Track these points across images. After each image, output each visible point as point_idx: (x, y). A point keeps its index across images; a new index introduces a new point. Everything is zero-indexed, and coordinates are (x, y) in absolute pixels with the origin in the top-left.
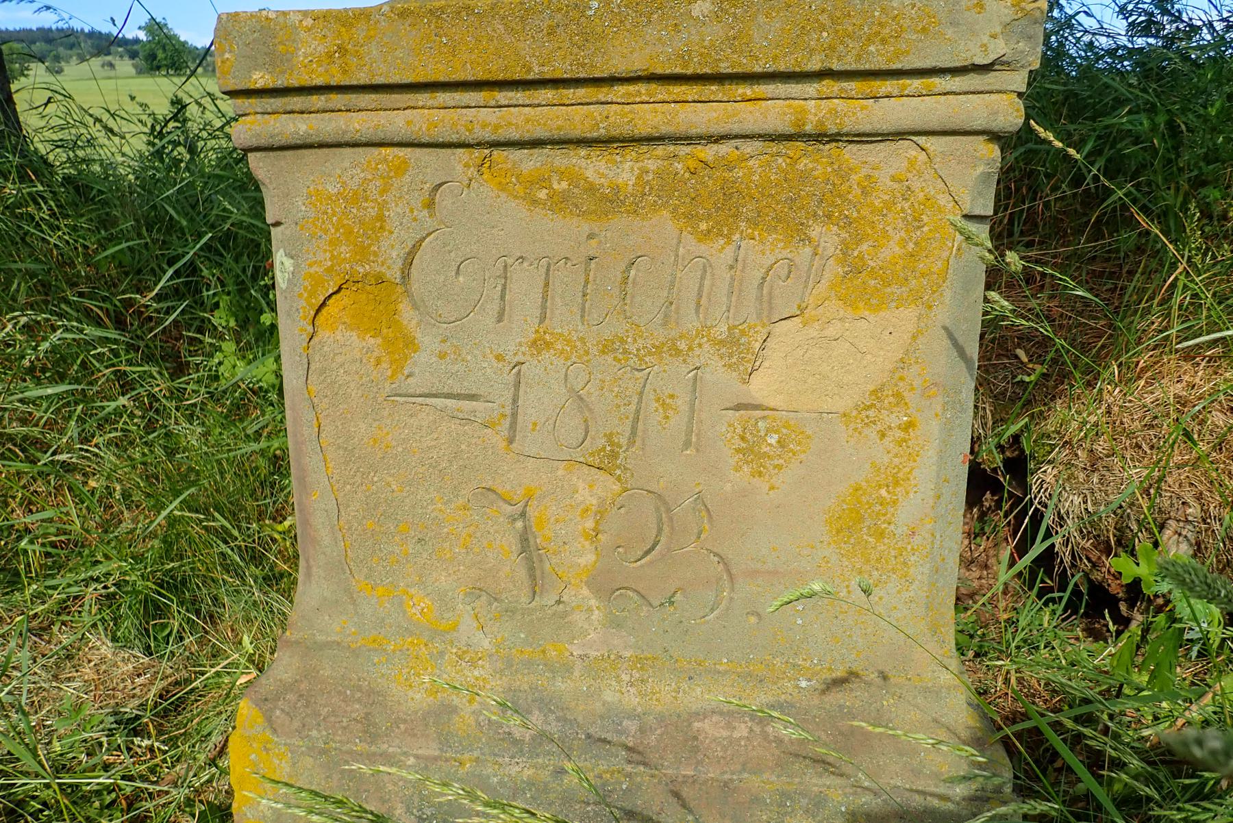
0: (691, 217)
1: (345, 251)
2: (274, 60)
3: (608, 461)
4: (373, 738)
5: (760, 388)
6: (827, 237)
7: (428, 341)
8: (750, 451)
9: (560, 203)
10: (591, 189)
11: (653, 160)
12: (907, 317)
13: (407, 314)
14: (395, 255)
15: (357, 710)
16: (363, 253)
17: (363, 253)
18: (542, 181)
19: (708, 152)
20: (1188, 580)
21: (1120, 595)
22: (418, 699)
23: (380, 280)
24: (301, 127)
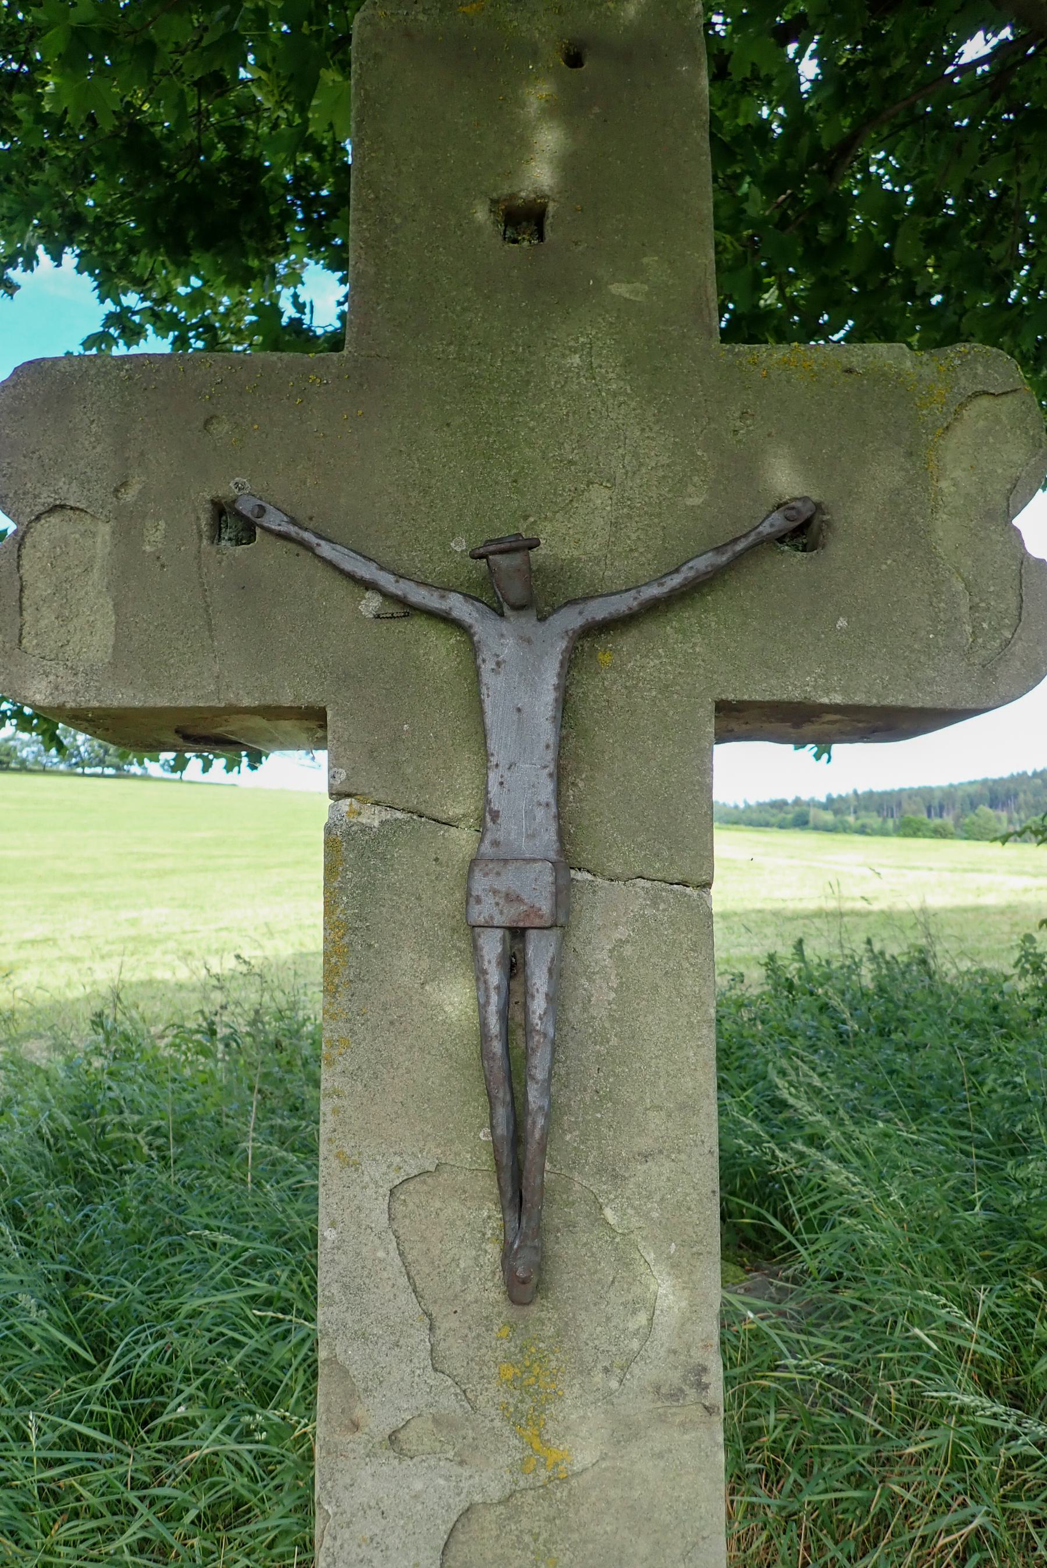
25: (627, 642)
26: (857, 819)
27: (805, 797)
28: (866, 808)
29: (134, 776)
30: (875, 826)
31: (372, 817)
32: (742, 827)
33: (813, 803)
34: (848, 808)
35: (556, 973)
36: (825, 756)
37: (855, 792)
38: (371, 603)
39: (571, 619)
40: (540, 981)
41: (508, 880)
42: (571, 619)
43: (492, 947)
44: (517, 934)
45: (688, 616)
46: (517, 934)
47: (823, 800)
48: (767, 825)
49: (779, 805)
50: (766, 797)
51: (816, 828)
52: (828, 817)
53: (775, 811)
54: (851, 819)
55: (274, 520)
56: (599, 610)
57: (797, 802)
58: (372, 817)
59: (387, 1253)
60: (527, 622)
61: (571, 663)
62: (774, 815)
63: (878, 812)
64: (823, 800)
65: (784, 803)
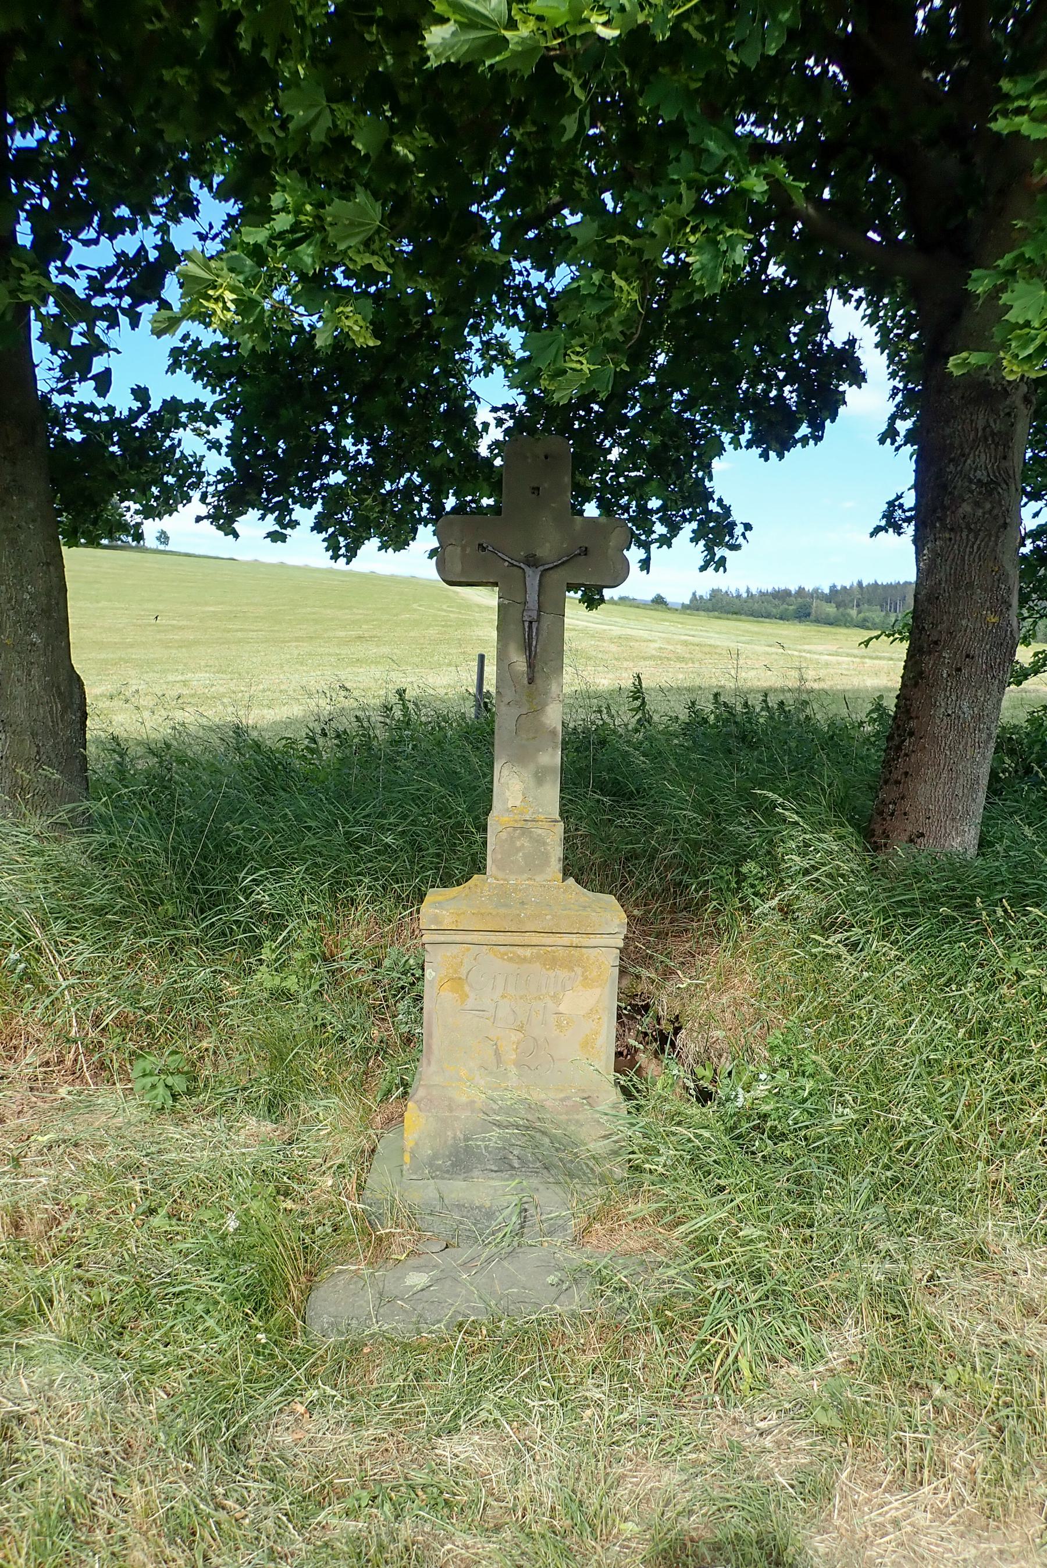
0: (545, 965)
1: (451, 971)
2: (437, 923)
3: (520, 1029)
4: (451, 1111)
5: (562, 1008)
6: (579, 970)
7: (472, 995)
8: (559, 1026)
9: (510, 960)
10: (519, 956)
11: (535, 950)
12: (598, 991)
13: (467, 988)
14: (465, 972)
15: (447, 1103)
16: (456, 972)
17: (456, 972)
18: (506, 954)
19: (549, 949)
20: (211, 292)
21: (932, 154)
22: (464, 1099)
23: (460, 978)
24: (442, 938)
25: (551, 572)
26: (859, 612)
27: (809, 587)
28: (869, 602)
29: (106, 547)
30: (877, 620)
31: (506, 602)
32: (743, 617)
33: (816, 594)
34: (852, 601)
35: (537, 629)
36: (722, 569)
37: (860, 584)
38: (506, 564)
39: (541, 568)
40: (534, 630)
41: (530, 613)
42: (541, 568)
43: (527, 624)
44: (531, 622)
45: (559, 570)
46: (531, 622)
47: (827, 591)
48: (768, 616)
49: (781, 595)
50: (768, 586)
51: (817, 621)
52: (831, 609)
53: (776, 602)
54: (853, 612)
55: (490, 548)
56: (547, 567)
57: (801, 591)
58: (506, 602)
59: (508, 674)
60: (534, 569)
61: (541, 576)
62: (776, 606)
63: (882, 606)
64: (827, 591)
65: (787, 593)
